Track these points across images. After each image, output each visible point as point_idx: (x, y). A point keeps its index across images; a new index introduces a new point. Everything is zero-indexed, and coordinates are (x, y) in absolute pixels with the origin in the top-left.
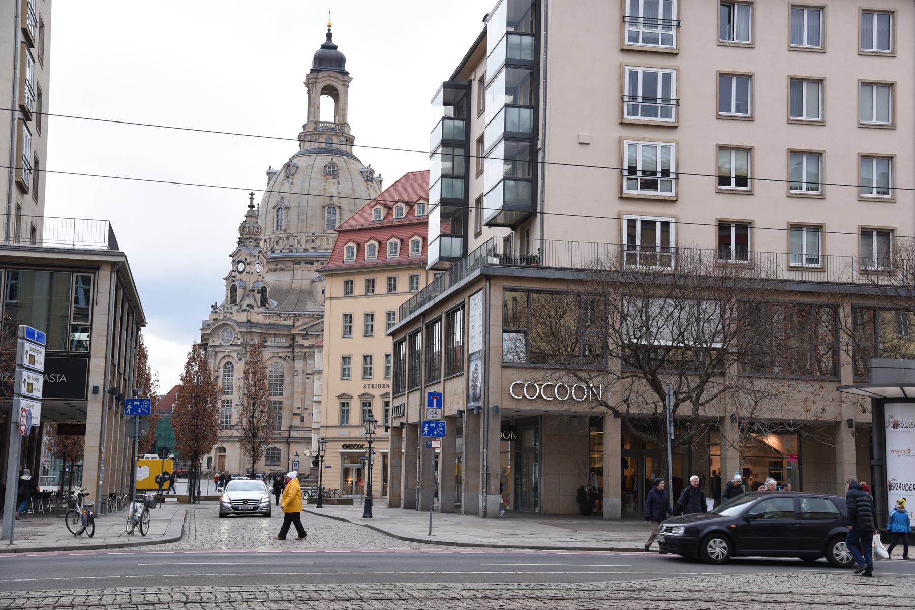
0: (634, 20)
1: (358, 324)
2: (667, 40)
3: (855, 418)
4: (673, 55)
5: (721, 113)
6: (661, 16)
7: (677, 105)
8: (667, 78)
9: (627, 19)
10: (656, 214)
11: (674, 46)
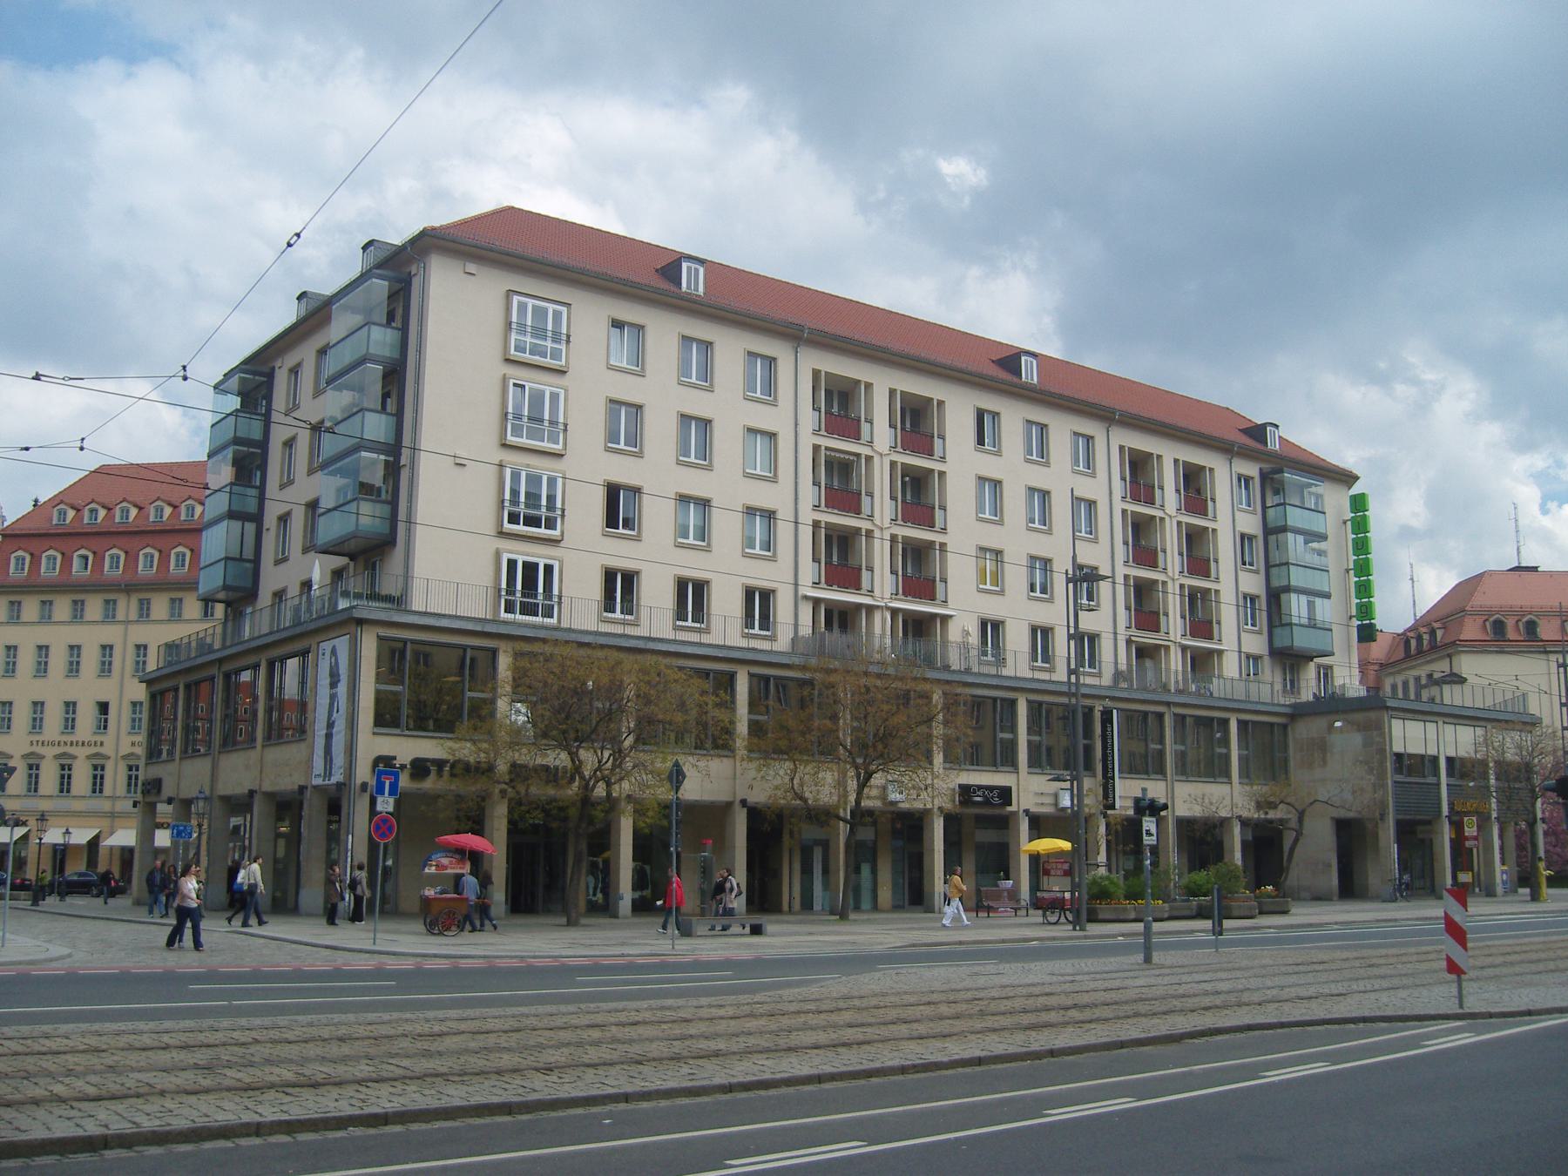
0: (522, 329)
1: (58, 660)
2: (556, 355)
3: (260, 786)
4: (561, 372)
5: (610, 445)
6: (550, 327)
7: (565, 430)
8: (554, 397)
9: (514, 326)
10: (540, 556)
11: (563, 363)
